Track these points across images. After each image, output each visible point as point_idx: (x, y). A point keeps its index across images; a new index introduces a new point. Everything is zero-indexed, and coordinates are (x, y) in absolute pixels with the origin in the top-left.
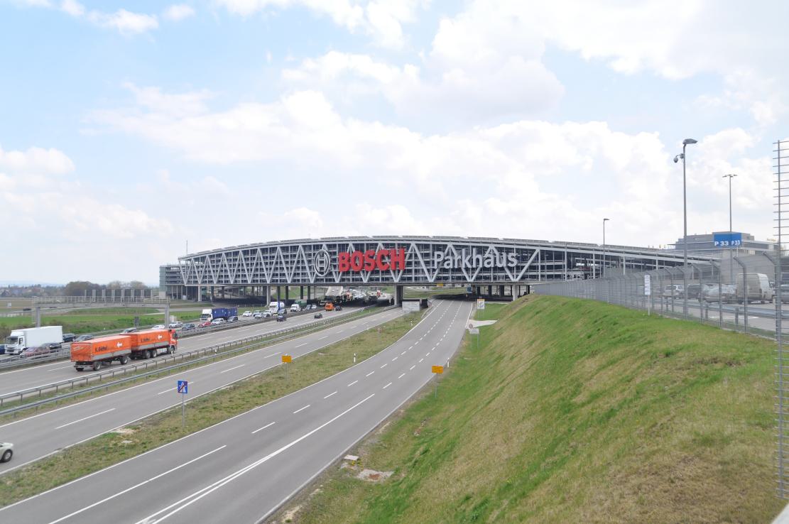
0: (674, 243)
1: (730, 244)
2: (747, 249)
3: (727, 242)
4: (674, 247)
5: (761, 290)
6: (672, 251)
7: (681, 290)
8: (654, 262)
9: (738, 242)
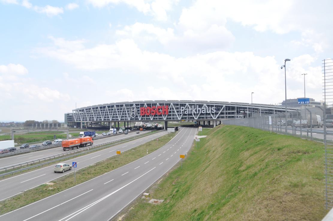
0: (281, 103)
1: (305, 103)
2: (312, 105)
3: (303, 102)
4: (281, 104)
5: (318, 122)
6: (280, 106)
7: (284, 122)
8: (273, 110)
9: (308, 102)
